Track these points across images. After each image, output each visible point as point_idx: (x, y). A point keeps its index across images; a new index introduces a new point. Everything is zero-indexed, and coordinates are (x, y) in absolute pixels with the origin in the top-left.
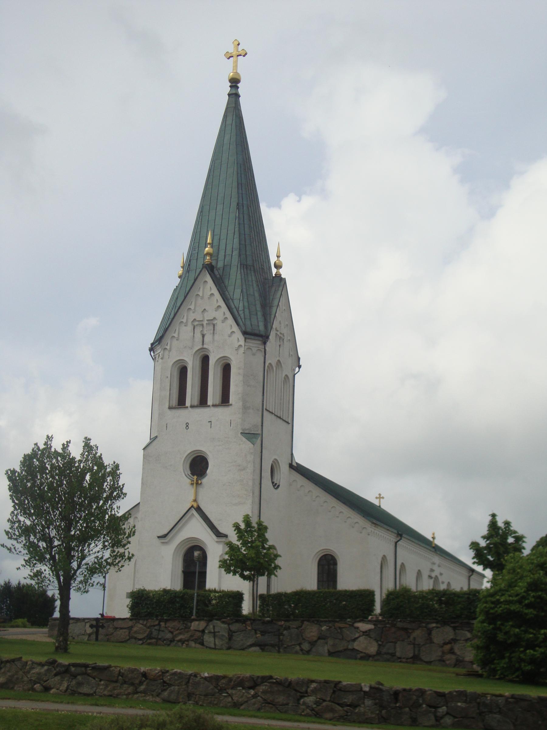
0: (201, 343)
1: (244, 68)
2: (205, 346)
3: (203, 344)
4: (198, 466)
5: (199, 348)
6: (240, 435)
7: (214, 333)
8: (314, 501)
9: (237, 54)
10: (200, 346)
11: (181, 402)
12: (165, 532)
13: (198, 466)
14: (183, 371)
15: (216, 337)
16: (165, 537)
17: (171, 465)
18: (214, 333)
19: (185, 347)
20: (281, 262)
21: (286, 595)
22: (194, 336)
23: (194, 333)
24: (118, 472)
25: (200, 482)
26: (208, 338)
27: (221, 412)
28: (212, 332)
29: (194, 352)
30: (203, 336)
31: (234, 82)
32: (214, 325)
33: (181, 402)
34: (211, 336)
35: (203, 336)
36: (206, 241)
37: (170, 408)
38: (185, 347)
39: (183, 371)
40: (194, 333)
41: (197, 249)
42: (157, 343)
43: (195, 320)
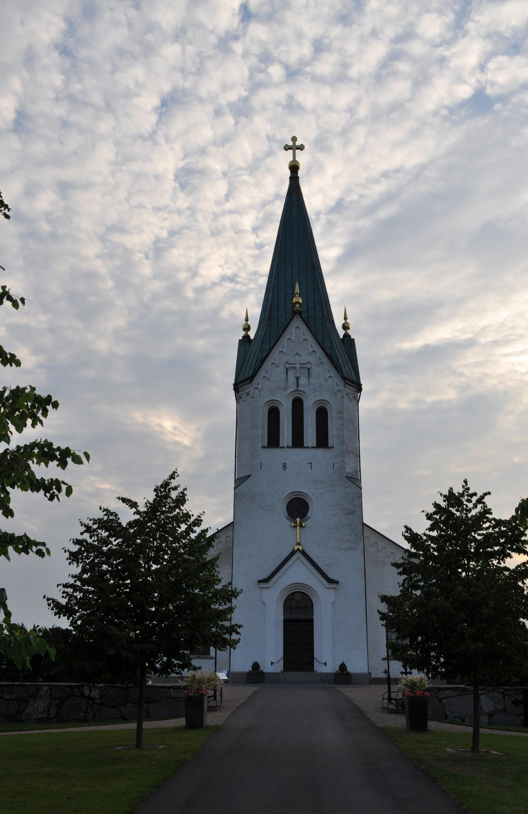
0: (296, 385)
1: (302, 158)
2: (300, 388)
3: (298, 386)
4: (298, 508)
5: (292, 390)
6: (344, 478)
7: (309, 377)
8: (380, 552)
9: (294, 147)
10: (295, 388)
11: (273, 441)
12: (265, 576)
13: (298, 508)
14: (274, 414)
15: (312, 380)
16: (268, 582)
17: (268, 506)
18: (309, 377)
19: (278, 388)
20: (348, 324)
21: (10, 617)
22: (287, 378)
23: (287, 375)
24: (127, 516)
25: (304, 525)
26: (303, 381)
27: (320, 452)
28: (307, 375)
29: (288, 393)
30: (298, 379)
31: (294, 168)
32: (309, 369)
33: (273, 441)
34: (306, 379)
35: (298, 379)
36: (293, 290)
37: (263, 447)
38: (278, 388)
39: (274, 414)
40: (287, 375)
41: (277, 301)
42: (248, 381)
43: (287, 362)
